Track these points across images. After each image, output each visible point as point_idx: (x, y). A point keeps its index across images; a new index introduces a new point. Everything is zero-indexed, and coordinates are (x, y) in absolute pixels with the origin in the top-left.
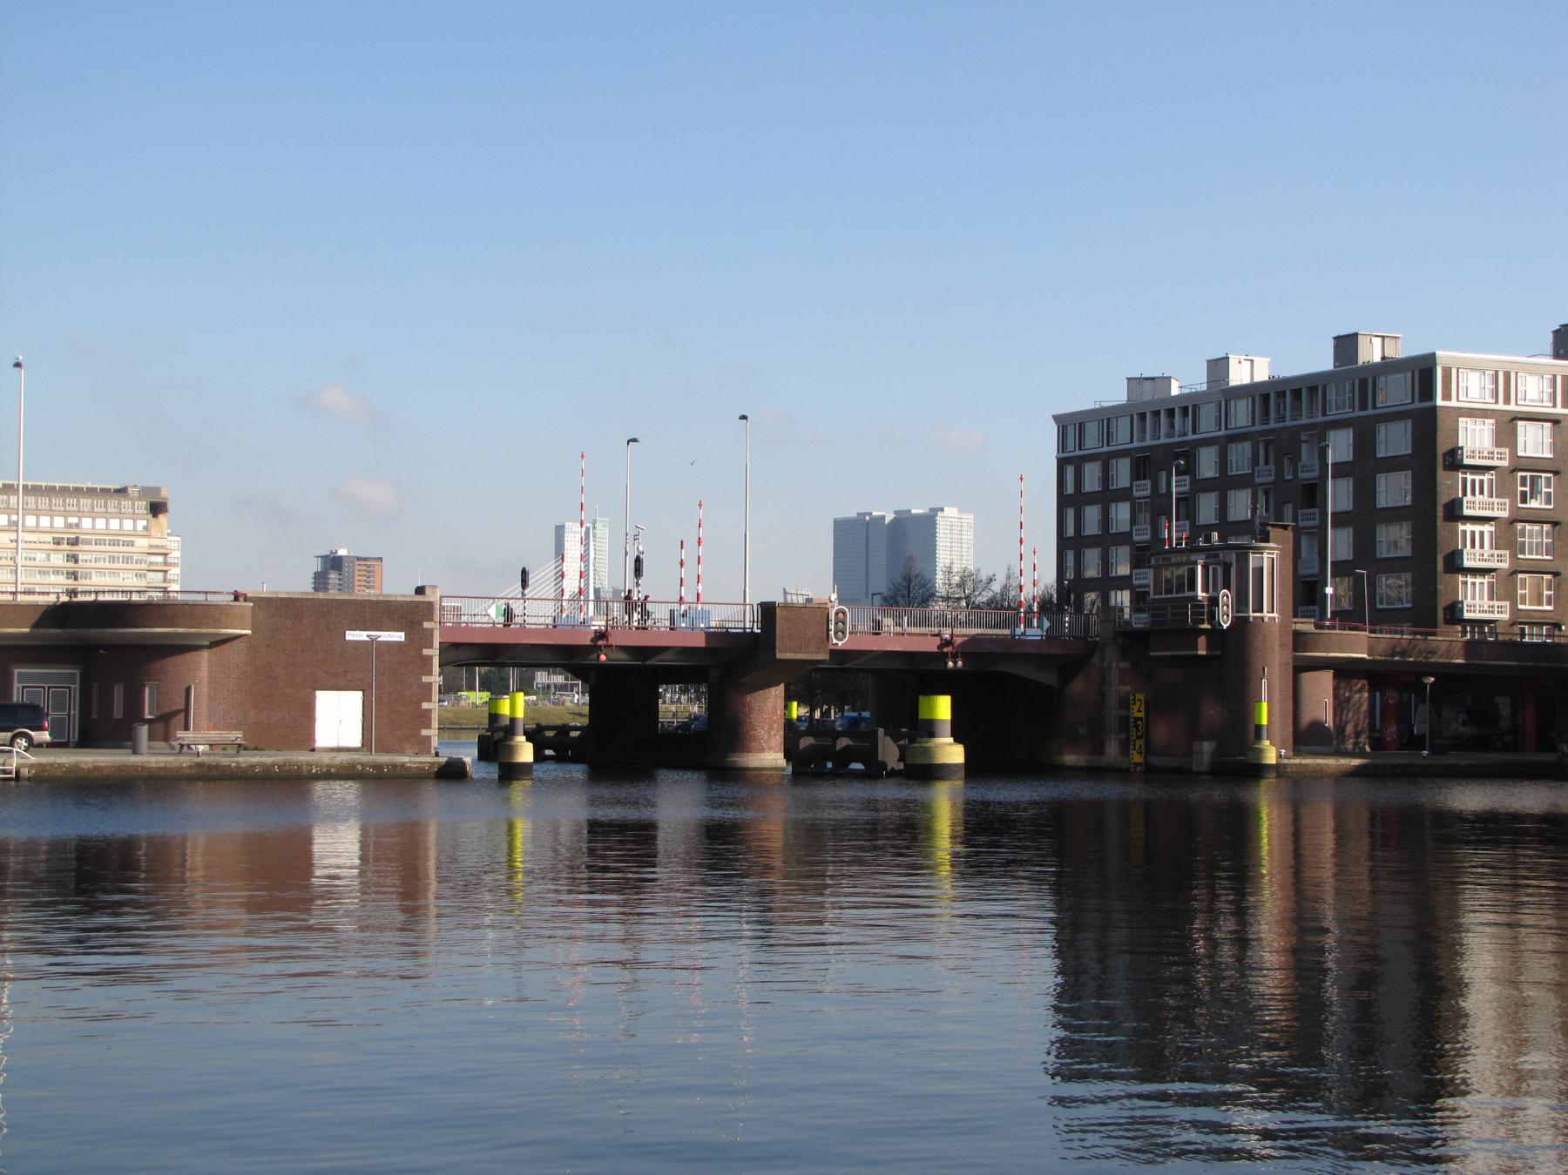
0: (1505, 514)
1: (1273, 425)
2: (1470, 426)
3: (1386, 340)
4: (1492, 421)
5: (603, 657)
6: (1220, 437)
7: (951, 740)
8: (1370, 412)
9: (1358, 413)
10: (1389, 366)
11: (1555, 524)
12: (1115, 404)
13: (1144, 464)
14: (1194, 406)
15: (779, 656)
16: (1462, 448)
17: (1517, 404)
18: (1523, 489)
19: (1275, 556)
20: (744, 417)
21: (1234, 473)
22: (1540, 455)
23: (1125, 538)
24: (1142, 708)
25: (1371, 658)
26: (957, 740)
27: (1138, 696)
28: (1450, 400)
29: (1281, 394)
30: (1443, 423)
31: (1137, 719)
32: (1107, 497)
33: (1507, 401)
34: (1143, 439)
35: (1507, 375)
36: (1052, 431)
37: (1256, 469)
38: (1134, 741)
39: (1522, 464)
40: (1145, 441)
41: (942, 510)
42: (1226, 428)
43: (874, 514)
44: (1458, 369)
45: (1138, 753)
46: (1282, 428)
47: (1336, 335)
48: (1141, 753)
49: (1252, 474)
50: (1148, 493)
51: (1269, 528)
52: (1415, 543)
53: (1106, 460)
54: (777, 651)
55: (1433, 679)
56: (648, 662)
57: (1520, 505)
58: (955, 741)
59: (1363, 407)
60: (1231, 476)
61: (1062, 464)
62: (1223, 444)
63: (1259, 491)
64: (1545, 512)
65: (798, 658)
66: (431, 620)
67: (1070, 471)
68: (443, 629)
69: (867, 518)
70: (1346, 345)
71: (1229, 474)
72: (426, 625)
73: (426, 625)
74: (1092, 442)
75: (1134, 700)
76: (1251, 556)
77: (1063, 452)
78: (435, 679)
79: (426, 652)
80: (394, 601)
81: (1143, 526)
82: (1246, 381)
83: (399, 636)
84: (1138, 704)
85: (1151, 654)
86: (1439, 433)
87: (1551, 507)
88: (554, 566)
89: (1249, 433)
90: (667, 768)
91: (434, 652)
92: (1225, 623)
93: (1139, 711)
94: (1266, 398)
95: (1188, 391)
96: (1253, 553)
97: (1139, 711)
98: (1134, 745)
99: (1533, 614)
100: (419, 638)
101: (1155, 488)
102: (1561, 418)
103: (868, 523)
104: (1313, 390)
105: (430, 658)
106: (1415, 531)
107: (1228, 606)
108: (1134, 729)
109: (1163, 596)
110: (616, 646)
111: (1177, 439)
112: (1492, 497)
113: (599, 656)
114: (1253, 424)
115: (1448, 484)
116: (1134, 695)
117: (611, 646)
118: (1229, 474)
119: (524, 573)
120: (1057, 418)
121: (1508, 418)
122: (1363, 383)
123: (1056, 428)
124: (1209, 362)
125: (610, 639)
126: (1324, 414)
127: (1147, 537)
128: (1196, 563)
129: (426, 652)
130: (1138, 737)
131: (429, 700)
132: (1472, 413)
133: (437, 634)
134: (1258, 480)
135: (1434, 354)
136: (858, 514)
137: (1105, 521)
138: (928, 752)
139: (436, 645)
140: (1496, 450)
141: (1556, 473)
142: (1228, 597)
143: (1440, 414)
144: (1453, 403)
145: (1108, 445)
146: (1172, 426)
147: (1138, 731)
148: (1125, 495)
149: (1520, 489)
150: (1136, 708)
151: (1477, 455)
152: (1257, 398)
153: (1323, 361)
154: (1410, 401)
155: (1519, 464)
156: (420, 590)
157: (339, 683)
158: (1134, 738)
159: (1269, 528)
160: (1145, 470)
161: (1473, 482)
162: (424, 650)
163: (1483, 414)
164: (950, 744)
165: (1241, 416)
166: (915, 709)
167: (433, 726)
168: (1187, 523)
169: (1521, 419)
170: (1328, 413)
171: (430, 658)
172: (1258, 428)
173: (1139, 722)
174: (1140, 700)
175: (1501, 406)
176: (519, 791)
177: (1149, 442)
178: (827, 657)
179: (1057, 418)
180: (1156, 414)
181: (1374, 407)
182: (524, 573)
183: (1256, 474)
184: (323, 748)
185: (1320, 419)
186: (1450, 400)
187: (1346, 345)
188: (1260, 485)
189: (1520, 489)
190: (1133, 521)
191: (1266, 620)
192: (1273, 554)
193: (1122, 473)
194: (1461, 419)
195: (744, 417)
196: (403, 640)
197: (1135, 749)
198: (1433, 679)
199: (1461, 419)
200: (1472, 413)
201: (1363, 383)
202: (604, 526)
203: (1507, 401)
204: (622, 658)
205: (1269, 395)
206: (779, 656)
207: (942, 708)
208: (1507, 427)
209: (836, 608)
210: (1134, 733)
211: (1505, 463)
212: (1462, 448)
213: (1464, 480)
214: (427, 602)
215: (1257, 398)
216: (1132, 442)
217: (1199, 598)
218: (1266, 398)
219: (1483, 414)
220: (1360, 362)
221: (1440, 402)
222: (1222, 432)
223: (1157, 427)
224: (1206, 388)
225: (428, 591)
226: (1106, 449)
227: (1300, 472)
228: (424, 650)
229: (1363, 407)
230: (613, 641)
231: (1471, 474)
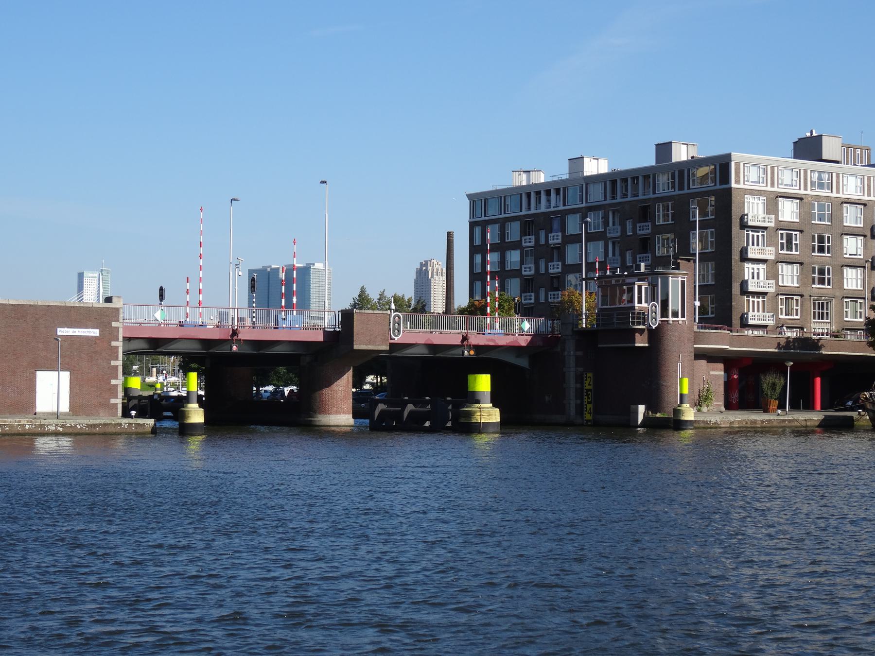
0: (772, 257)
1: (619, 200)
2: (751, 200)
3: (689, 146)
4: (765, 198)
5: (234, 348)
6: (582, 208)
7: (491, 405)
8: (686, 191)
9: (677, 192)
10: (695, 163)
11: (801, 264)
12: (506, 187)
13: (529, 225)
14: (564, 189)
15: (356, 347)
16: (747, 215)
17: (778, 187)
18: (782, 241)
19: (685, 279)
20: (324, 182)
21: (593, 231)
22: (792, 220)
23: (516, 273)
24: (591, 383)
25: (779, 351)
26: (495, 406)
27: (590, 375)
28: (684, 190)
29: (625, 180)
30: (735, 198)
31: (588, 390)
32: (502, 247)
33: (773, 185)
34: (529, 209)
35: (772, 168)
36: (466, 204)
37: (608, 228)
38: (586, 405)
39: (782, 225)
40: (530, 210)
41: (314, 265)
42: (587, 202)
43: (273, 267)
44: (744, 164)
45: (588, 413)
46: (626, 202)
47: (657, 143)
48: (590, 413)
49: (605, 232)
50: (533, 244)
51: (679, 261)
52: (716, 276)
53: (503, 223)
54: (354, 343)
55: (792, 363)
56: (211, 351)
57: (780, 252)
58: (493, 406)
59: (681, 188)
60: (590, 233)
61: (472, 225)
62: (584, 213)
63: (609, 242)
64: (794, 257)
65: (360, 348)
66: (118, 321)
67: (478, 230)
68: (125, 328)
69: (269, 270)
70: (664, 150)
71: (506, 241)
72: (114, 324)
73: (114, 324)
74: (493, 212)
75: (586, 377)
76: (670, 279)
77: (473, 218)
78: (119, 363)
79: (114, 344)
80: (91, 307)
81: (529, 266)
82: (595, 173)
83: (95, 332)
84: (589, 379)
85: (599, 346)
86: (733, 205)
87: (798, 253)
88: (76, 298)
89: (603, 205)
90: (276, 426)
91: (119, 344)
92: (655, 325)
93: (589, 385)
94: (614, 183)
95: (557, 179)
96: (672, 277)
97: (589, 385)
98: (586, 408)
99: (788, 321)
100: (109, 333)
101: (537, 240)
102: (803, 197)
103: (269, 273)
104: (646, 177)
105: (117, 348)
106: (717, 268)
107: (656, 313)
108: (586, 397)
109: (609, 307)
110: (243, 340)
111: (552, 209)
112: (764, 246)
113: (231, 347)
114: (605, 199)
115: (739, 238)
116: (586, 374)
117: (240, 340)
118: (506, 241)
119: (161, 290)
120: (469, 196)
121: (773, 196)
122: (681, 173)
123: (469, 202)
124: (657, 145)
125: (239, 335)
126: (654, 193)
127: (533, 273)
128: (634, 284)
129: (114, 344)
130: (589, 403)
131: (116, 378)
132: (752, 192)
133: (121, 330)
134: (609, 236)
135: (731, 154)
136: (307, 264)
137: (503, 262)
138: (470, 414)
139: (121, 339)
140: (767, 216)
141: (801, 231)
142: (656, 307)
143: (734, 194)
144: (741, 186)
145: (505, 213)
146: (549, 201)
147: (589, 398)
148: (516, 245)
149: (780, 241)
150: (587, 382)
151: (757, 219)
152: (608, 183)
153: (649, 160)
154: (713, 184)
155: (781, 226)
156: (108, 300)
157: (51, 366)
158: (586, 403)
159: (679, 261)
160: (529, 229)
161: (753, 236)
162: (112, 342)
163: (759, 193)
164: (490, 407)
165: (596, 195)
166: (465, 383)
167: (119, 397)
168: (560, 263)
169: (781, 197)
170: (657, 192)
171: (117, 348)
172: (609, 201)
173: (589, 393)
174: (590, 377)
175: (769, 188)
176: (195, 443)
177: (533, 211)
178: (388, 348)
179: (469, 196)
180: (538, 193)
181: (689, 188)
182: (161, 290)
183: (608, 232)
184: (44, 413)
185: (652, 196)
186: (684, 190)
187: (664, 150)
188: (610, 238)
189: (780, 241)
190: (522, 262)
191: (680, 322)
192: (684, 278)
193: (514, 232)
194: (746, 196)
195: (324, 182)
196: (98, 335)
197: (586, 411)
198: (792, 363)
199: (746, 196)
200: (752, 192)
201: (681, 173)
202: (108, 273)
203: (773, 185)
204: (248, 350)
205: (616, 181)
206: (356, 347)
207: (483, 383)
208: (773, 201)
209: (393, 316)
210: (586, 400)
211: (772, 225)
212: (747, 215)
213: (748, 235)
214: (114, 308)
215: (608, 183)
216: (521, 211)
217: (636, 308)
218: (614, 183)
219: (759, 193)
220: (674, 160)
221: (733, 185)
222: (584, 205)
223: (538, 201)
224: (568, 177)
225: (114, 300)
226: (503, 216)
227: (638, 230)
228: (112, 342)
229: (681, 188)
230: (241, 336)
231: (752, 231)
